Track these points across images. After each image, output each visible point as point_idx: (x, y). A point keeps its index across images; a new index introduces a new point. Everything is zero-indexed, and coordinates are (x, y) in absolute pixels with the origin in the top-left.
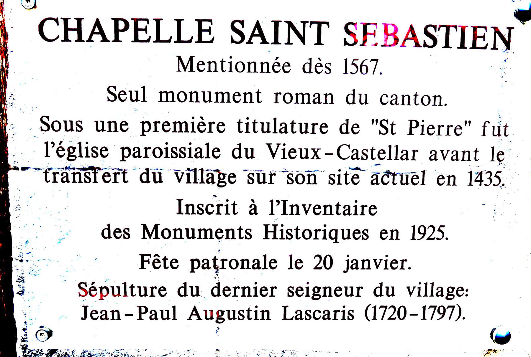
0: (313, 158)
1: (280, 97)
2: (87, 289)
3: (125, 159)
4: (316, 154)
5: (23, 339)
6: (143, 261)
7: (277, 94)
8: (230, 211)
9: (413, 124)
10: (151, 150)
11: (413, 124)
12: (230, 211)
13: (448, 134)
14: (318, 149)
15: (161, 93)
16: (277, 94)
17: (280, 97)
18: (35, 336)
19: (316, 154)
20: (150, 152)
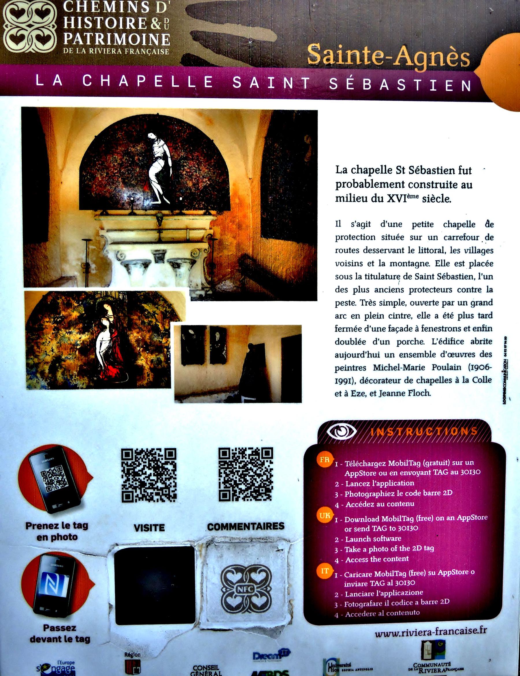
0: (393, 195)
1: (338, 251)
2: (414, 170)
3: (338, 188)
4: (391, 198)
5: (279, 657)
6: (434, 367)
7: (336, 249)
8: (402, 252)
9: (434, 366)
10: (346, 184)
11: (434, 366)
12: (402, 252)
13: (479, 279)
14: (389, 201)
15: (337, 197)
16: (336, 249)
17: (338, 251)
18: (267, 566)
19: (391, 198)
20: (345, 185)
